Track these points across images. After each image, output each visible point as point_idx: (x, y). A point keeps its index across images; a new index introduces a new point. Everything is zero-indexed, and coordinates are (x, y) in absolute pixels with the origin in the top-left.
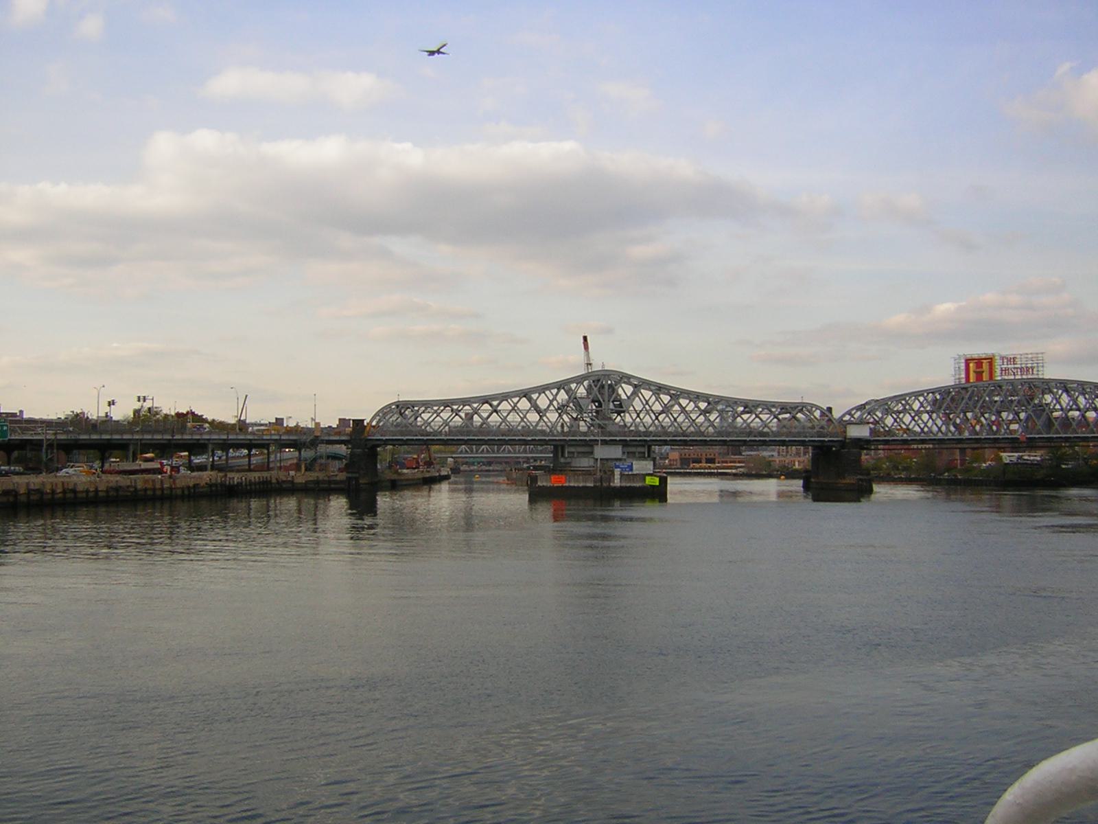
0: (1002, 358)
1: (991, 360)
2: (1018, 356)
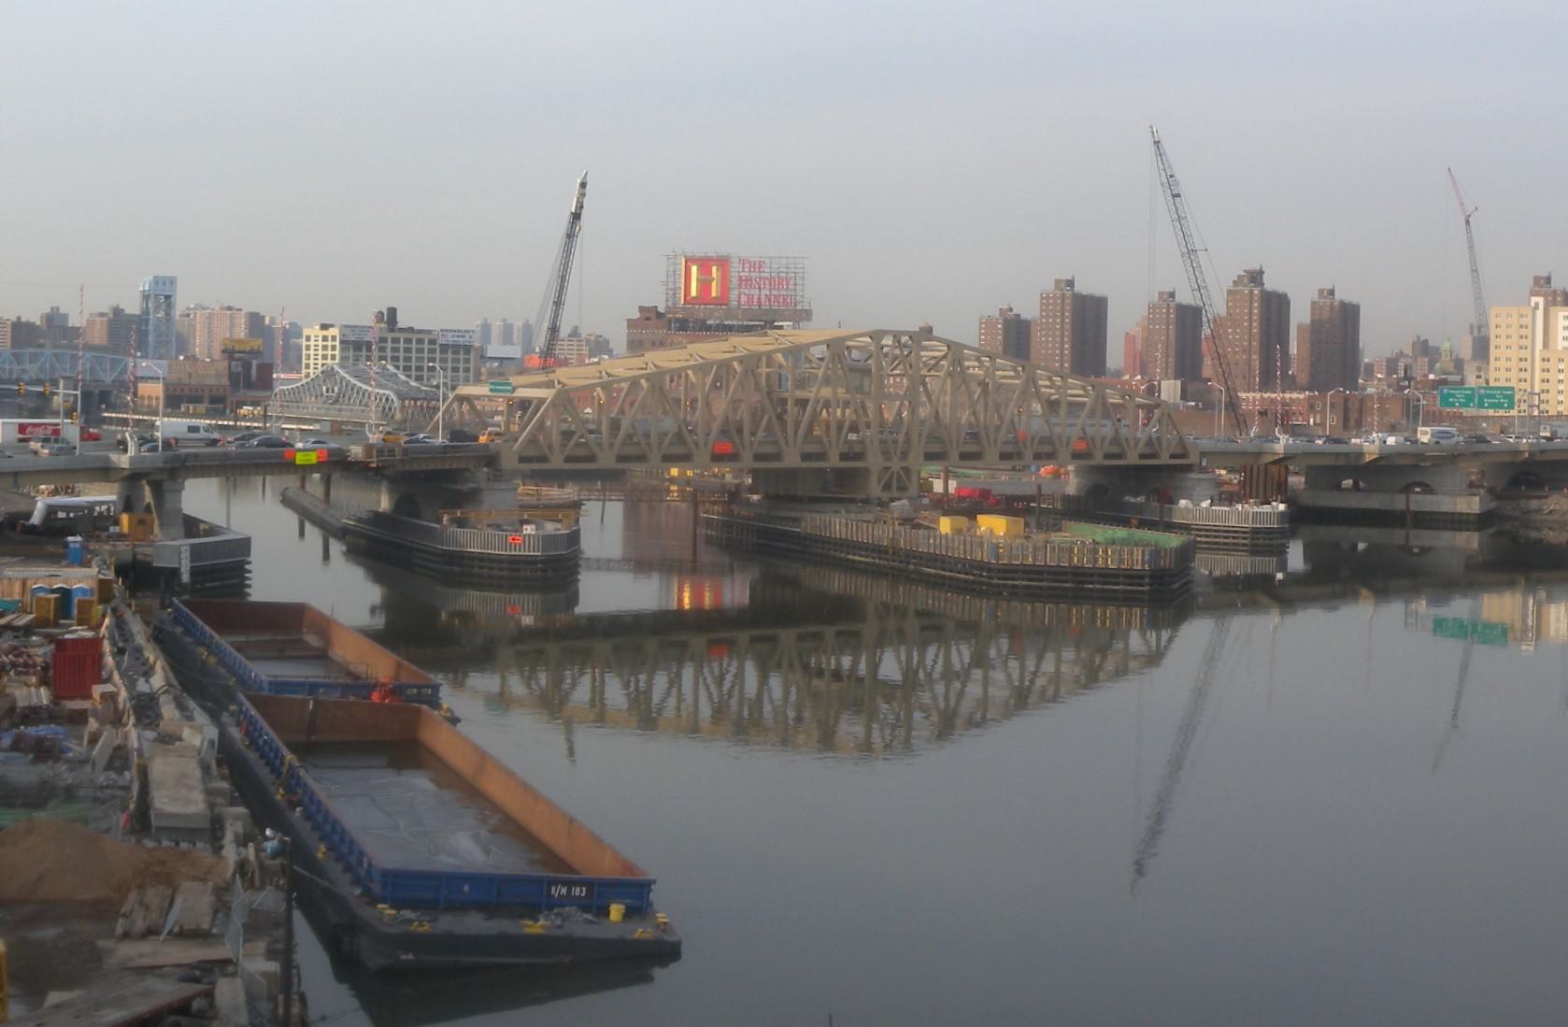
0: (743, 261)
1: (723, 262)
2: (767, 261)
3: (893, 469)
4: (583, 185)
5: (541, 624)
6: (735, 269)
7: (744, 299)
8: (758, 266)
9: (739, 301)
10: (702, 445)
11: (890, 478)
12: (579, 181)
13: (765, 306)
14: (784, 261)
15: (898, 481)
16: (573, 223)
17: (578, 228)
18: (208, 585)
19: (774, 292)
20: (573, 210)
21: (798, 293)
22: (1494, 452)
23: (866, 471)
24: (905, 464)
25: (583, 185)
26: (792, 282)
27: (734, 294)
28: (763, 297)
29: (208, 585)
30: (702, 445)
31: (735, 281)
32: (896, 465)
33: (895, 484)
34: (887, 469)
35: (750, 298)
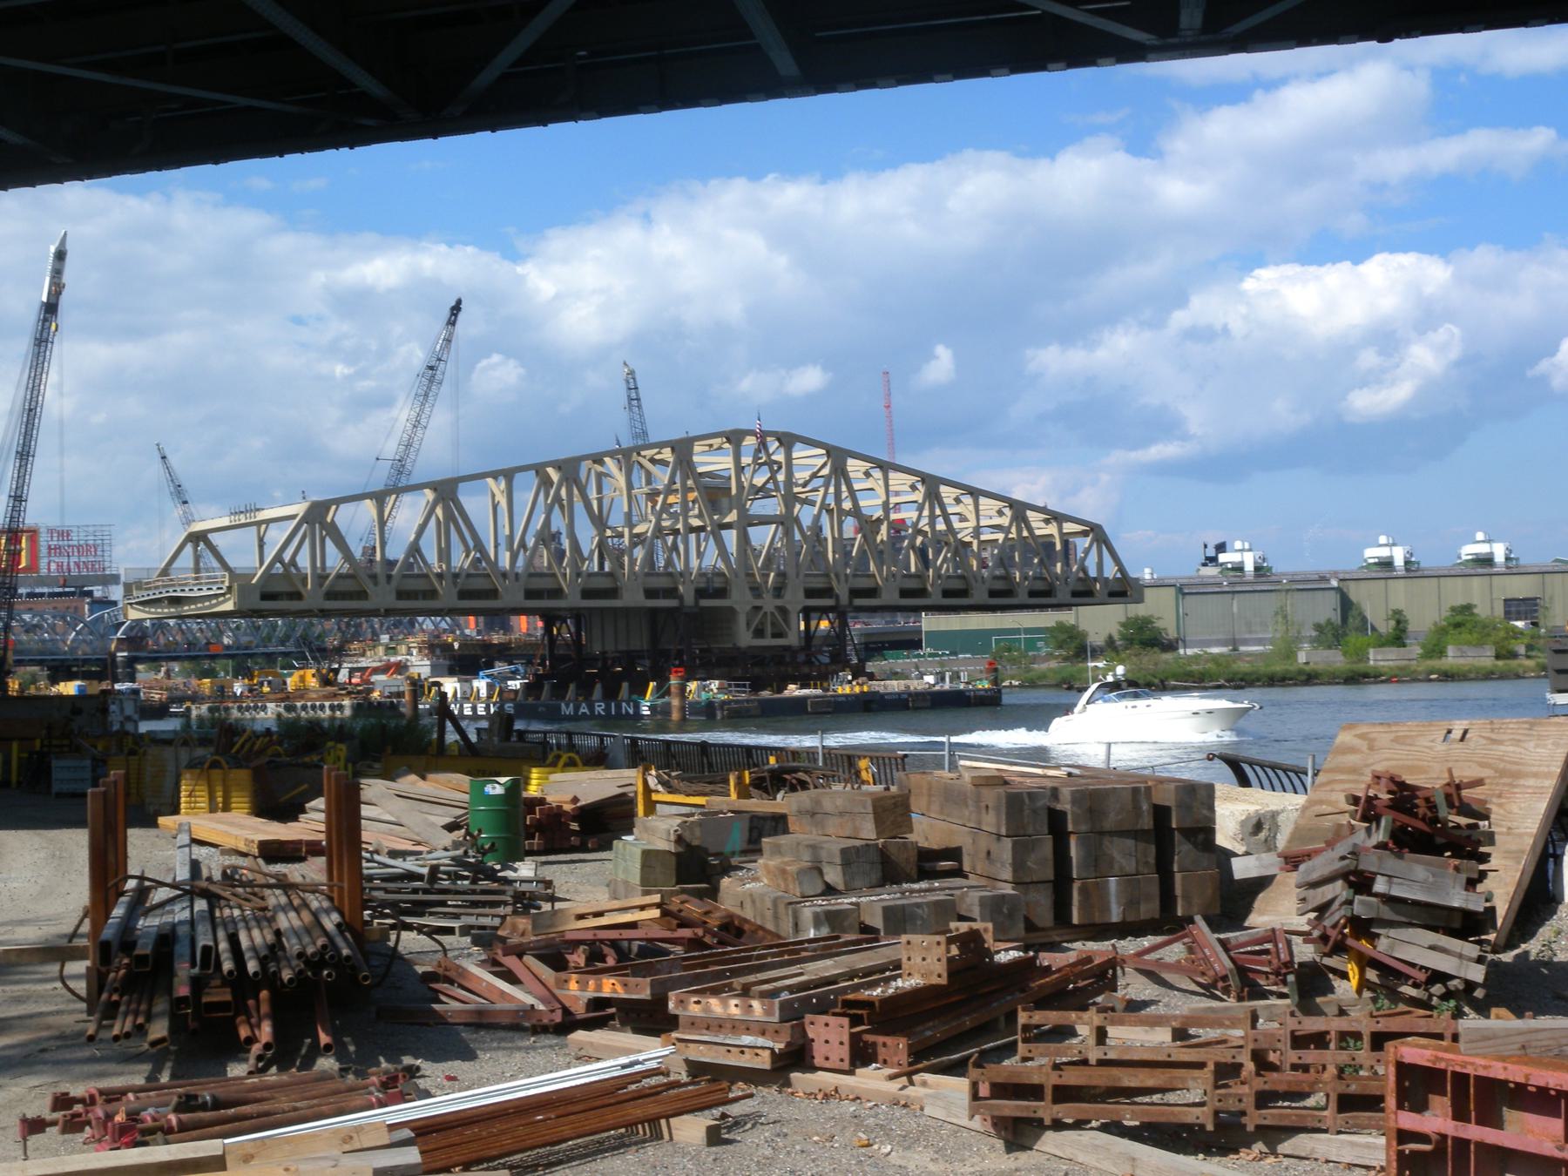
0: (51, 531)
2: (75, 529)
3: (765, 610)
4: (60, 256)
5: (525, 768)
6: (44, 540)
7: (53, 566)
8: (64, 534)
9: (49, 569)
10: (382, 579)
11: (762, 623)
12: (53, 249)
13: (74, 572)
14: (91, 529)
15: (773, 624)
16: (45, 320)
17: (53, 327)
18: (655, 53)
19: (83, 559)
20: (45, 299)
21: (106, 558)
22: (1021, 706)
23: (731, 611)
24: (779, 602)
25: (60, 256)
26: (99, 549)
27: (43, 563)
28: (72, 564)
29: (655, 53)
30: (382, 579)
31: (43, 551)
32: (769, 603)
33: (769, 630)
34: (757, 609)
35: (60, 566)
